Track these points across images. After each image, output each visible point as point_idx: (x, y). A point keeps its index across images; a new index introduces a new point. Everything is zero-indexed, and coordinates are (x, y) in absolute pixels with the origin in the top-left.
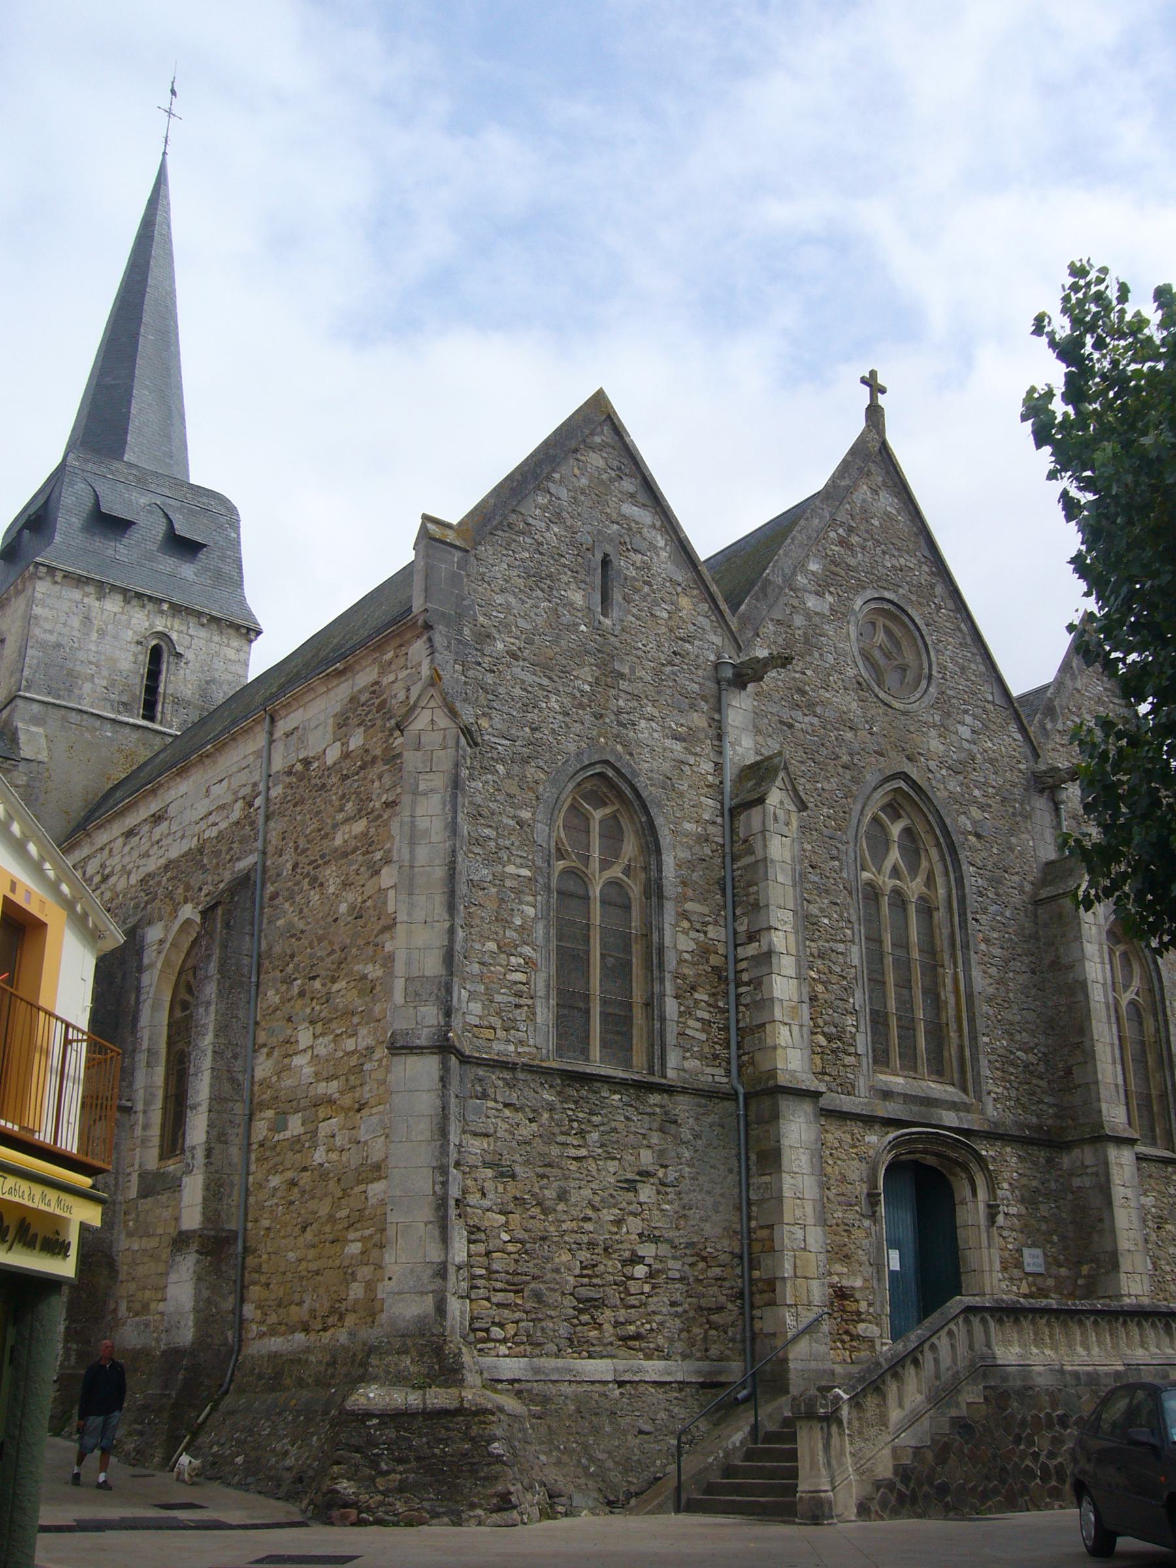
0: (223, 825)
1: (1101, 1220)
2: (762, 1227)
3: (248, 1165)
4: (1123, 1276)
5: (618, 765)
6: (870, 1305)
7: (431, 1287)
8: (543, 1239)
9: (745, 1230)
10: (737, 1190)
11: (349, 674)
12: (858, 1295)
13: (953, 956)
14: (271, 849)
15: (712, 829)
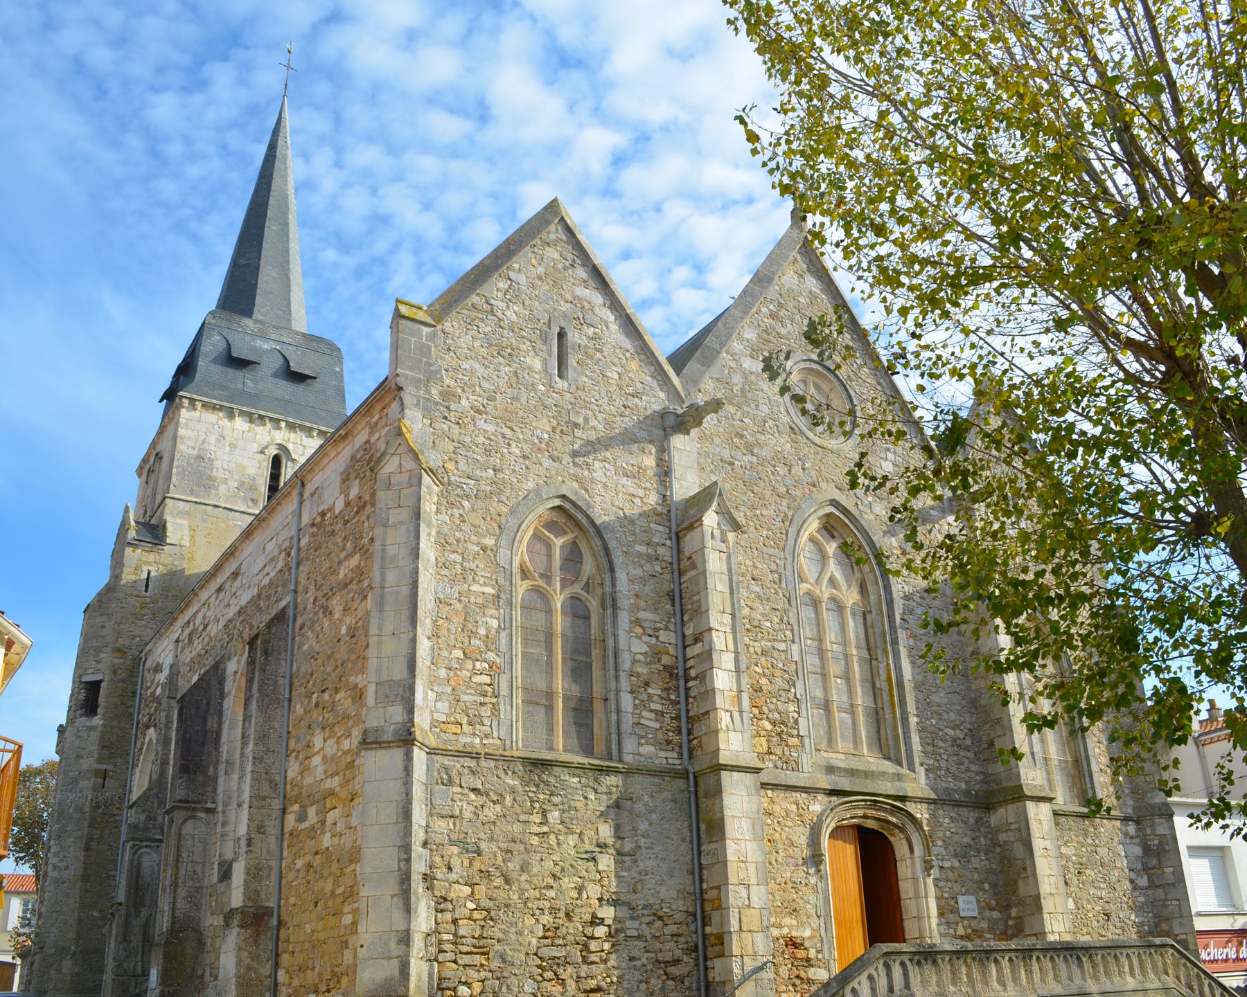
0: (272, 574)
1: (1024, 869)
2: (711, 888)
3: (282, 850)
4: (1046, 916)
5: (573, 498)
6: (818, 951)
7: (394, 954)
8: (507, 906)
9: (698, 891)
10: (689, 857)
11: (350, 438)
12: (807, 944)
13: (885, 651)
14: (300, 588)
15: (661, 551)
